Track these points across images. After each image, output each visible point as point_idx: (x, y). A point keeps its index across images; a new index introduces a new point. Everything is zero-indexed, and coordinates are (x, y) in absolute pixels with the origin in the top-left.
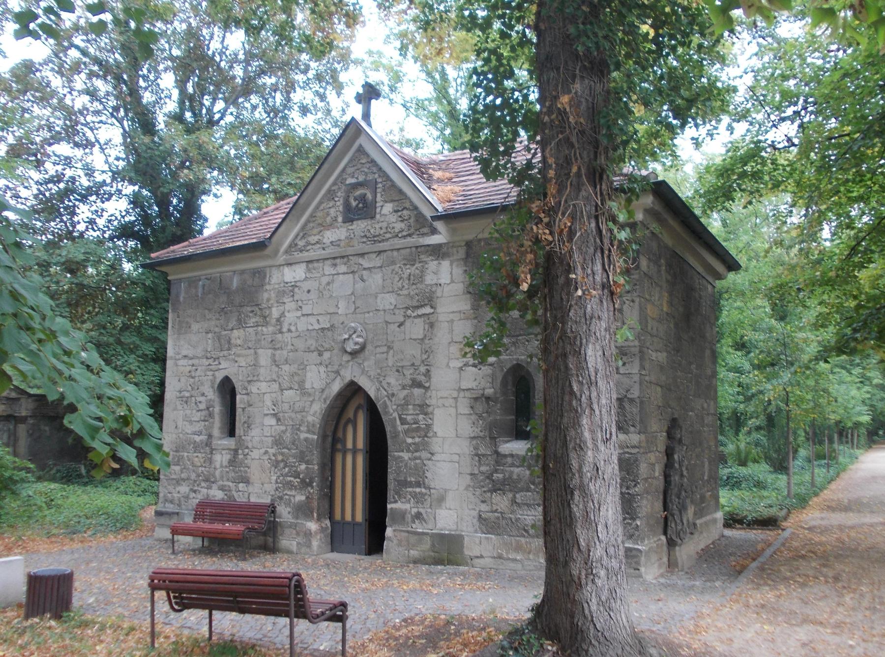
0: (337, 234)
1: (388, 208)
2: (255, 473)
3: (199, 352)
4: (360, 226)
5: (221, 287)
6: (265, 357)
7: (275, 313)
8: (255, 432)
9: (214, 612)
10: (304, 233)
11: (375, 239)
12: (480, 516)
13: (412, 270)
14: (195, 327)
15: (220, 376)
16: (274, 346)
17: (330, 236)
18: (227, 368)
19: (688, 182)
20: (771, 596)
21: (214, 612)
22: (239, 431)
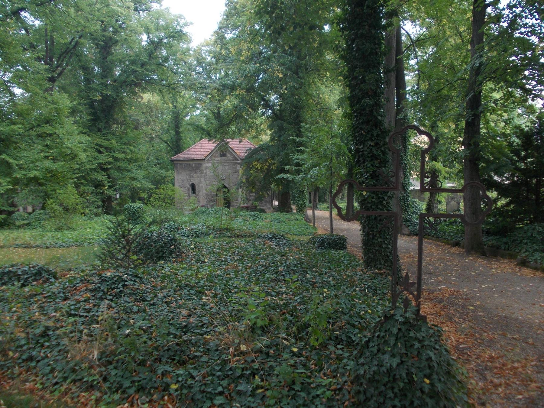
0: (219, 158)
1: (229, 155)
2: (201, 200)
3: (185, 178)
4: (223, 158)
5: (190, 165)
6: (202, 180)
7: (205, 172)
8: (201, 193)
9: (426, 243)
10: (211, 157)
11: (227, 161)
12: (35, 48)
13: (235, 166)
14: (183, 173)
15: (191, 183)
16: (204, 177)
17: (217, 159)
18: (192, 181)
19: (276, 106)
20: (336, 129)
21: (426, 243)
22: (196, 192)
